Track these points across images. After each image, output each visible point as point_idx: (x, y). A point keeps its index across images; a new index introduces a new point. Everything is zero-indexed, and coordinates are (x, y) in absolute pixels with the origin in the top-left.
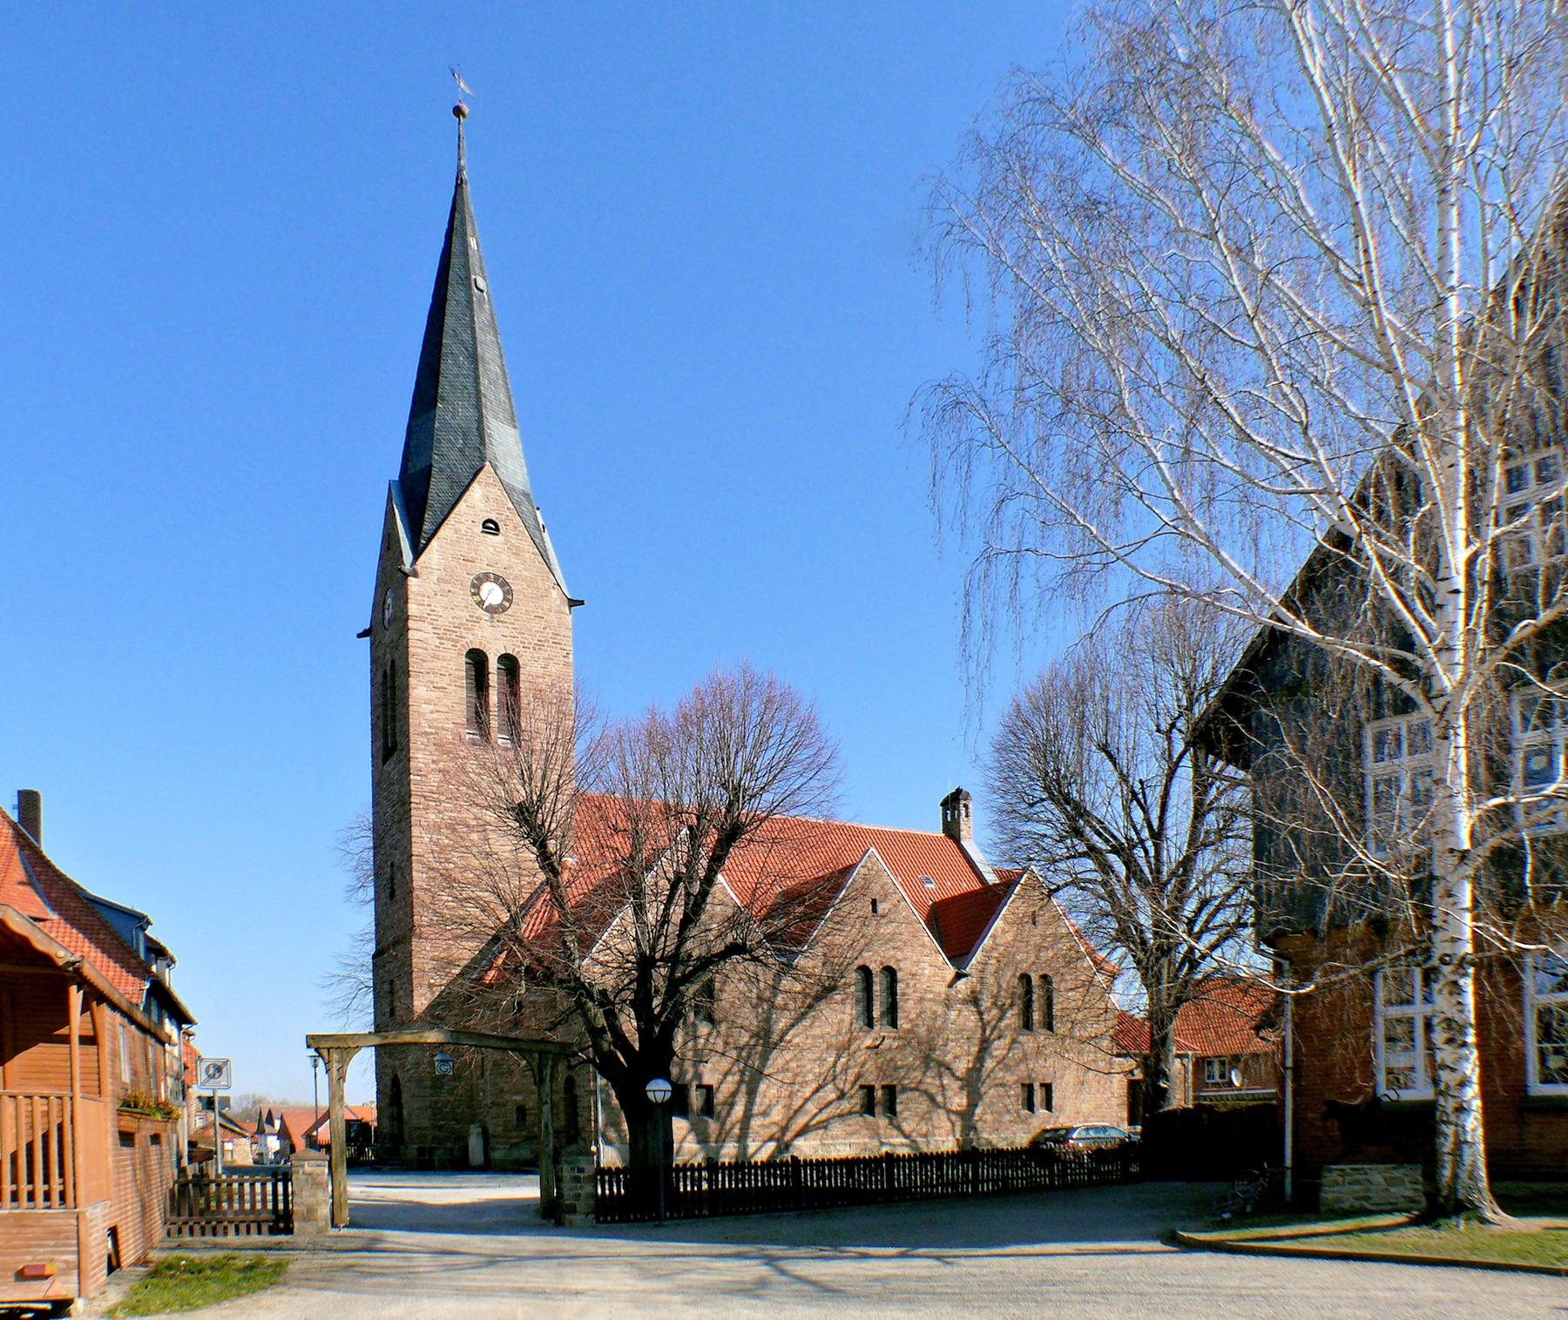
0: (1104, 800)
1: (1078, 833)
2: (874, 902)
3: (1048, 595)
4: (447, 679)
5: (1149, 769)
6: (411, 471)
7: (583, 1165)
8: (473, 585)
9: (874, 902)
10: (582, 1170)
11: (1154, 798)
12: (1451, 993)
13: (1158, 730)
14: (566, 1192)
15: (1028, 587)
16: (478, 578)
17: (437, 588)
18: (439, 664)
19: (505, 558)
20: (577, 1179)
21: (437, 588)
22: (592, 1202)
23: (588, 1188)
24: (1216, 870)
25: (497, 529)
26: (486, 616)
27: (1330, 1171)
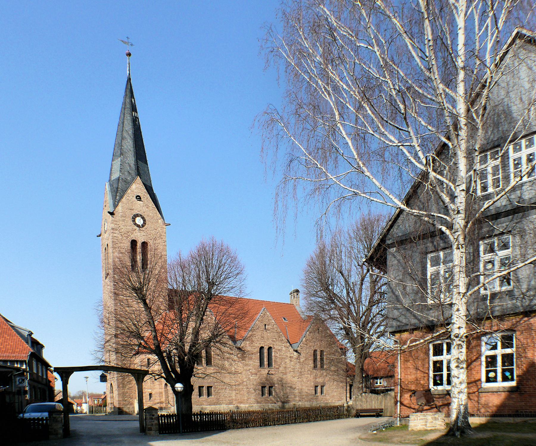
0: (340, 289)
1: (333, 302)
2: (265, 325)
3: (308, 197)
5: (355, 278)
6: (112, 179)
7: (154, 413)
8: (133, 218)
9: (265, 325)
10: (153, 415)
11: (357, 291)
12: (458, 348)
13: (358, 265)
14: (148, 423)
15: (300, 193)
16: (134, 215)
19: (145, 209)
20: (152, 419)
22: (157, 427)
23: (156, 422)
24: (378, 314)
25: (141, 199)
26: (138, 228)
27: (413, 415)
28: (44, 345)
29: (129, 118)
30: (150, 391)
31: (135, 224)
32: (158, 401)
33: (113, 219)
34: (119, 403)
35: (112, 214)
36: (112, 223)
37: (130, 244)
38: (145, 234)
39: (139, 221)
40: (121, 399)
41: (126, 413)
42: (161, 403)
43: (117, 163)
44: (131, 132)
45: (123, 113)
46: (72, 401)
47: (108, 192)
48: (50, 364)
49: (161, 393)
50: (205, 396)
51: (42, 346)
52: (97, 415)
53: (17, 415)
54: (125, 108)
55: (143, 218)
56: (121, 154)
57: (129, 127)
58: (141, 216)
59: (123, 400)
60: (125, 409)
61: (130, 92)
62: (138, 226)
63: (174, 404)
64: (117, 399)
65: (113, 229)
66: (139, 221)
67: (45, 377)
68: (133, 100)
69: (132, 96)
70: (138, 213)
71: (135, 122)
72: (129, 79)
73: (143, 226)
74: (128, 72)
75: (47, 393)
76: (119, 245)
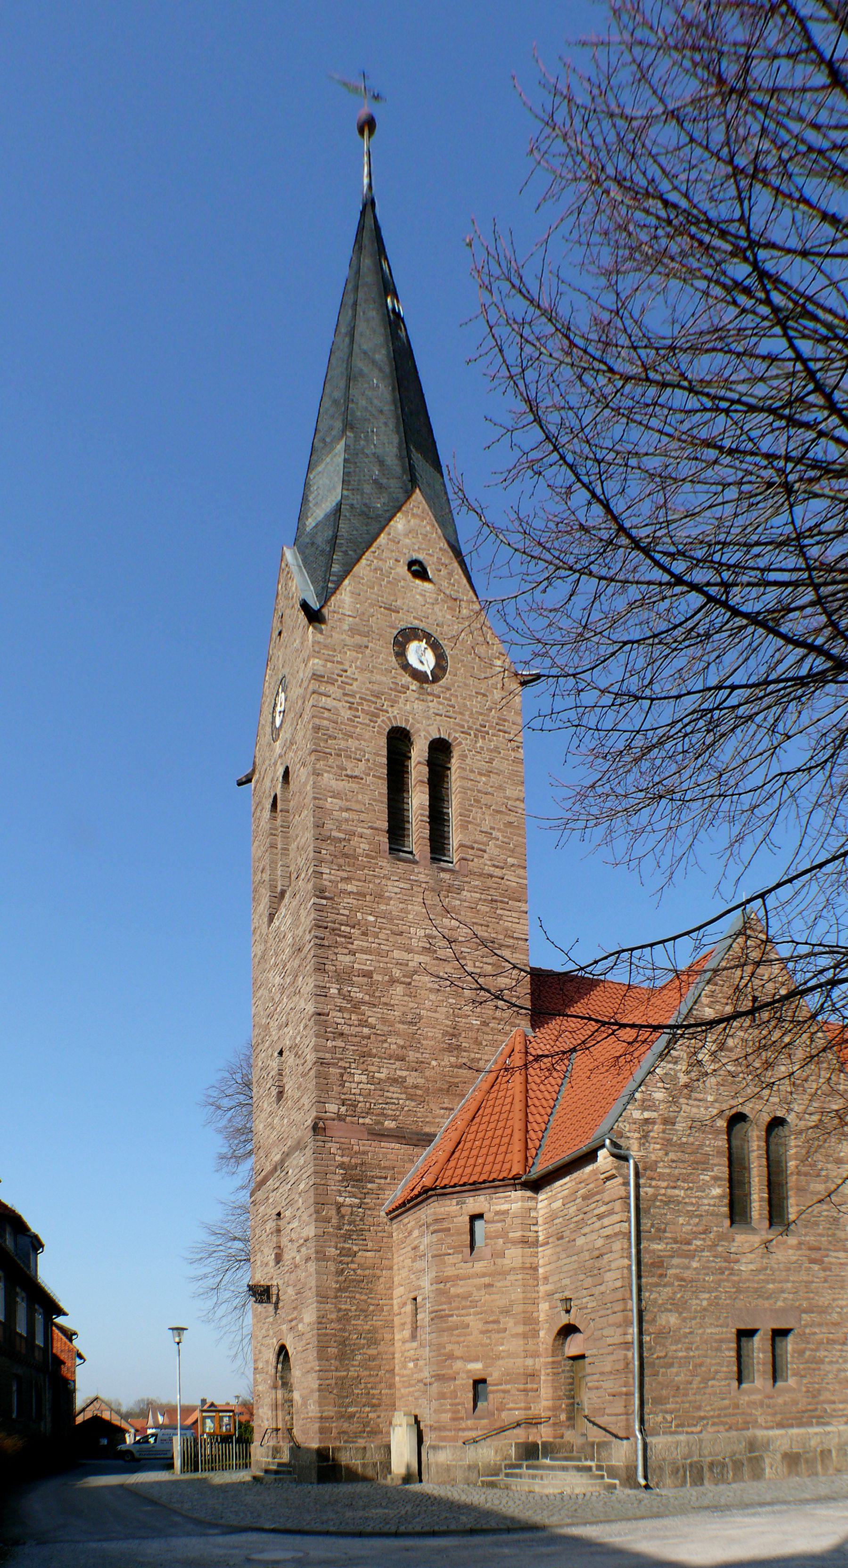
4: (362, 765)
17: (349, 641)
18: (352, 744)
21: (349, 641)
26: (414, 685)
28: (43, 1240)
29: (373, 314)
30: (477, 1367)
31: (406, 667)
32: (518, 1415)
33: (319, 637)
34: (322, 1431)
35: (314, 617)
36: (316, 654)
37: (383, 742)
38: (442, 710)
39: (420, 657)
40: (330, 1411)
41: (352, 1476)
42: (532, 1422)
43: (333, 464)
44: (381, 356)
45: (350, 304)
46: (124, 1425)
47: (294, 569)
48: (63, 1305)
49: (533, 1375)
50: (760, 1381)
51: (42, 1246)
52: (219, 1478)
53: (122, 1447)
54: (356, 289)
55: (435, 646)
56: (348, 425)
57: (372, 339)
58: (428, 636)
59: (341, 1416)
60: (346, 1458)
61: (370, 237)
62: (418, 675)
63: (629, 1427)
64: (313, 1409)
65: (316, 677)
66: (420, 657)
67: (39, 1342)
68: (385, 266)
69: (381, 251)
70: (416, 623)
71: (394, 323)
72: (369, 204)
73: (436, 679)
74: (366, 181)
75: (48, 1396)
76: (343, 744)
